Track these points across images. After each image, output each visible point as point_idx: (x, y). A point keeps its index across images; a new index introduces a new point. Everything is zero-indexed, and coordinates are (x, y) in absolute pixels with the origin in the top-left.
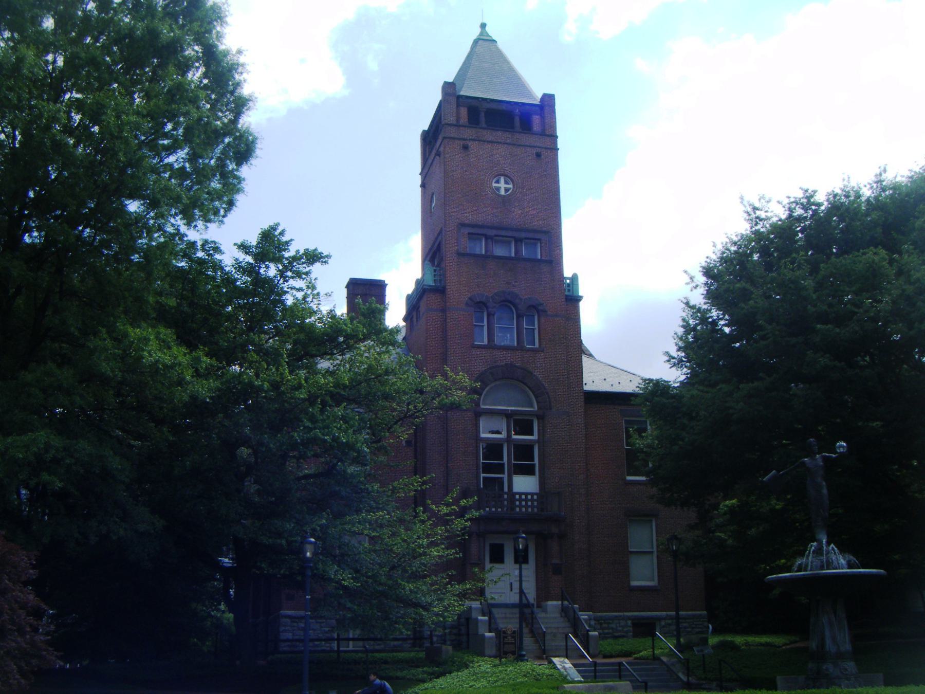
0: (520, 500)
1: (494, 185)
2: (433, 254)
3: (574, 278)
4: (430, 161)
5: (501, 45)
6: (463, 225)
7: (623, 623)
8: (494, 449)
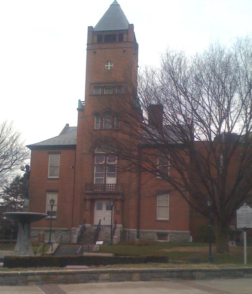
0: (108, 187)
7: (152, 234)
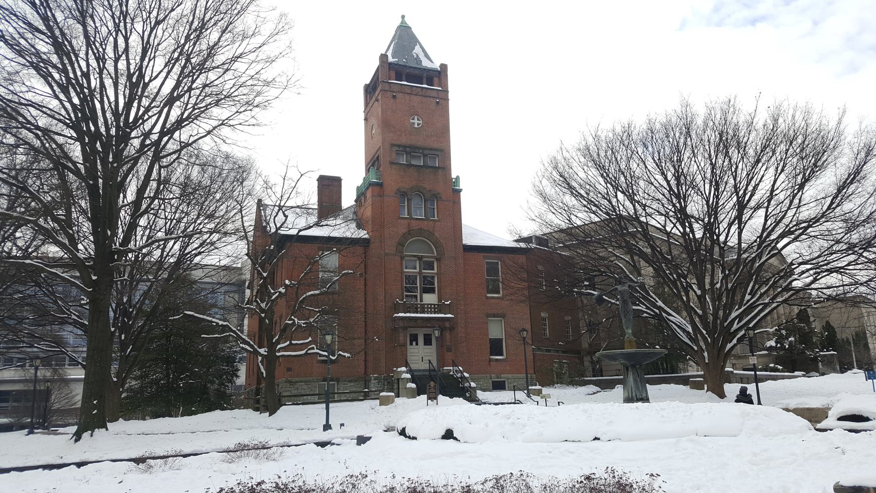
2: (373, 163)
3: (458, 178)
4: (370, 105)
5: (414, 30)
8: (411, 279)
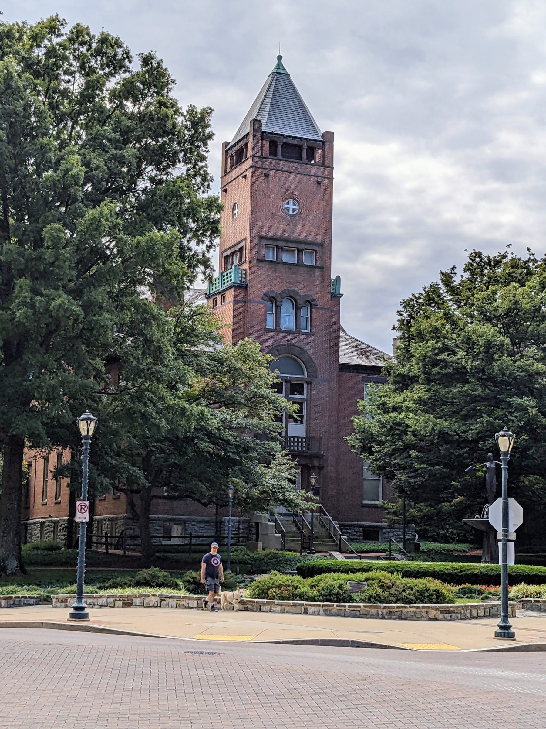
1: (286, 206)
5: (292, 78)
6: (261, 238)
7: (357, 529)
